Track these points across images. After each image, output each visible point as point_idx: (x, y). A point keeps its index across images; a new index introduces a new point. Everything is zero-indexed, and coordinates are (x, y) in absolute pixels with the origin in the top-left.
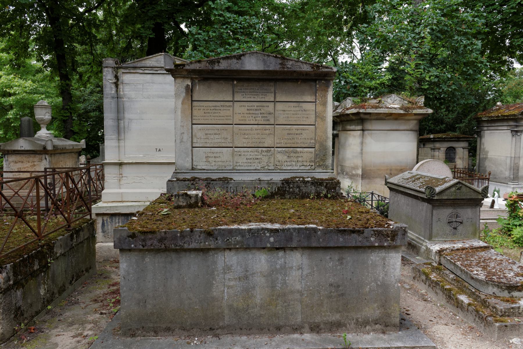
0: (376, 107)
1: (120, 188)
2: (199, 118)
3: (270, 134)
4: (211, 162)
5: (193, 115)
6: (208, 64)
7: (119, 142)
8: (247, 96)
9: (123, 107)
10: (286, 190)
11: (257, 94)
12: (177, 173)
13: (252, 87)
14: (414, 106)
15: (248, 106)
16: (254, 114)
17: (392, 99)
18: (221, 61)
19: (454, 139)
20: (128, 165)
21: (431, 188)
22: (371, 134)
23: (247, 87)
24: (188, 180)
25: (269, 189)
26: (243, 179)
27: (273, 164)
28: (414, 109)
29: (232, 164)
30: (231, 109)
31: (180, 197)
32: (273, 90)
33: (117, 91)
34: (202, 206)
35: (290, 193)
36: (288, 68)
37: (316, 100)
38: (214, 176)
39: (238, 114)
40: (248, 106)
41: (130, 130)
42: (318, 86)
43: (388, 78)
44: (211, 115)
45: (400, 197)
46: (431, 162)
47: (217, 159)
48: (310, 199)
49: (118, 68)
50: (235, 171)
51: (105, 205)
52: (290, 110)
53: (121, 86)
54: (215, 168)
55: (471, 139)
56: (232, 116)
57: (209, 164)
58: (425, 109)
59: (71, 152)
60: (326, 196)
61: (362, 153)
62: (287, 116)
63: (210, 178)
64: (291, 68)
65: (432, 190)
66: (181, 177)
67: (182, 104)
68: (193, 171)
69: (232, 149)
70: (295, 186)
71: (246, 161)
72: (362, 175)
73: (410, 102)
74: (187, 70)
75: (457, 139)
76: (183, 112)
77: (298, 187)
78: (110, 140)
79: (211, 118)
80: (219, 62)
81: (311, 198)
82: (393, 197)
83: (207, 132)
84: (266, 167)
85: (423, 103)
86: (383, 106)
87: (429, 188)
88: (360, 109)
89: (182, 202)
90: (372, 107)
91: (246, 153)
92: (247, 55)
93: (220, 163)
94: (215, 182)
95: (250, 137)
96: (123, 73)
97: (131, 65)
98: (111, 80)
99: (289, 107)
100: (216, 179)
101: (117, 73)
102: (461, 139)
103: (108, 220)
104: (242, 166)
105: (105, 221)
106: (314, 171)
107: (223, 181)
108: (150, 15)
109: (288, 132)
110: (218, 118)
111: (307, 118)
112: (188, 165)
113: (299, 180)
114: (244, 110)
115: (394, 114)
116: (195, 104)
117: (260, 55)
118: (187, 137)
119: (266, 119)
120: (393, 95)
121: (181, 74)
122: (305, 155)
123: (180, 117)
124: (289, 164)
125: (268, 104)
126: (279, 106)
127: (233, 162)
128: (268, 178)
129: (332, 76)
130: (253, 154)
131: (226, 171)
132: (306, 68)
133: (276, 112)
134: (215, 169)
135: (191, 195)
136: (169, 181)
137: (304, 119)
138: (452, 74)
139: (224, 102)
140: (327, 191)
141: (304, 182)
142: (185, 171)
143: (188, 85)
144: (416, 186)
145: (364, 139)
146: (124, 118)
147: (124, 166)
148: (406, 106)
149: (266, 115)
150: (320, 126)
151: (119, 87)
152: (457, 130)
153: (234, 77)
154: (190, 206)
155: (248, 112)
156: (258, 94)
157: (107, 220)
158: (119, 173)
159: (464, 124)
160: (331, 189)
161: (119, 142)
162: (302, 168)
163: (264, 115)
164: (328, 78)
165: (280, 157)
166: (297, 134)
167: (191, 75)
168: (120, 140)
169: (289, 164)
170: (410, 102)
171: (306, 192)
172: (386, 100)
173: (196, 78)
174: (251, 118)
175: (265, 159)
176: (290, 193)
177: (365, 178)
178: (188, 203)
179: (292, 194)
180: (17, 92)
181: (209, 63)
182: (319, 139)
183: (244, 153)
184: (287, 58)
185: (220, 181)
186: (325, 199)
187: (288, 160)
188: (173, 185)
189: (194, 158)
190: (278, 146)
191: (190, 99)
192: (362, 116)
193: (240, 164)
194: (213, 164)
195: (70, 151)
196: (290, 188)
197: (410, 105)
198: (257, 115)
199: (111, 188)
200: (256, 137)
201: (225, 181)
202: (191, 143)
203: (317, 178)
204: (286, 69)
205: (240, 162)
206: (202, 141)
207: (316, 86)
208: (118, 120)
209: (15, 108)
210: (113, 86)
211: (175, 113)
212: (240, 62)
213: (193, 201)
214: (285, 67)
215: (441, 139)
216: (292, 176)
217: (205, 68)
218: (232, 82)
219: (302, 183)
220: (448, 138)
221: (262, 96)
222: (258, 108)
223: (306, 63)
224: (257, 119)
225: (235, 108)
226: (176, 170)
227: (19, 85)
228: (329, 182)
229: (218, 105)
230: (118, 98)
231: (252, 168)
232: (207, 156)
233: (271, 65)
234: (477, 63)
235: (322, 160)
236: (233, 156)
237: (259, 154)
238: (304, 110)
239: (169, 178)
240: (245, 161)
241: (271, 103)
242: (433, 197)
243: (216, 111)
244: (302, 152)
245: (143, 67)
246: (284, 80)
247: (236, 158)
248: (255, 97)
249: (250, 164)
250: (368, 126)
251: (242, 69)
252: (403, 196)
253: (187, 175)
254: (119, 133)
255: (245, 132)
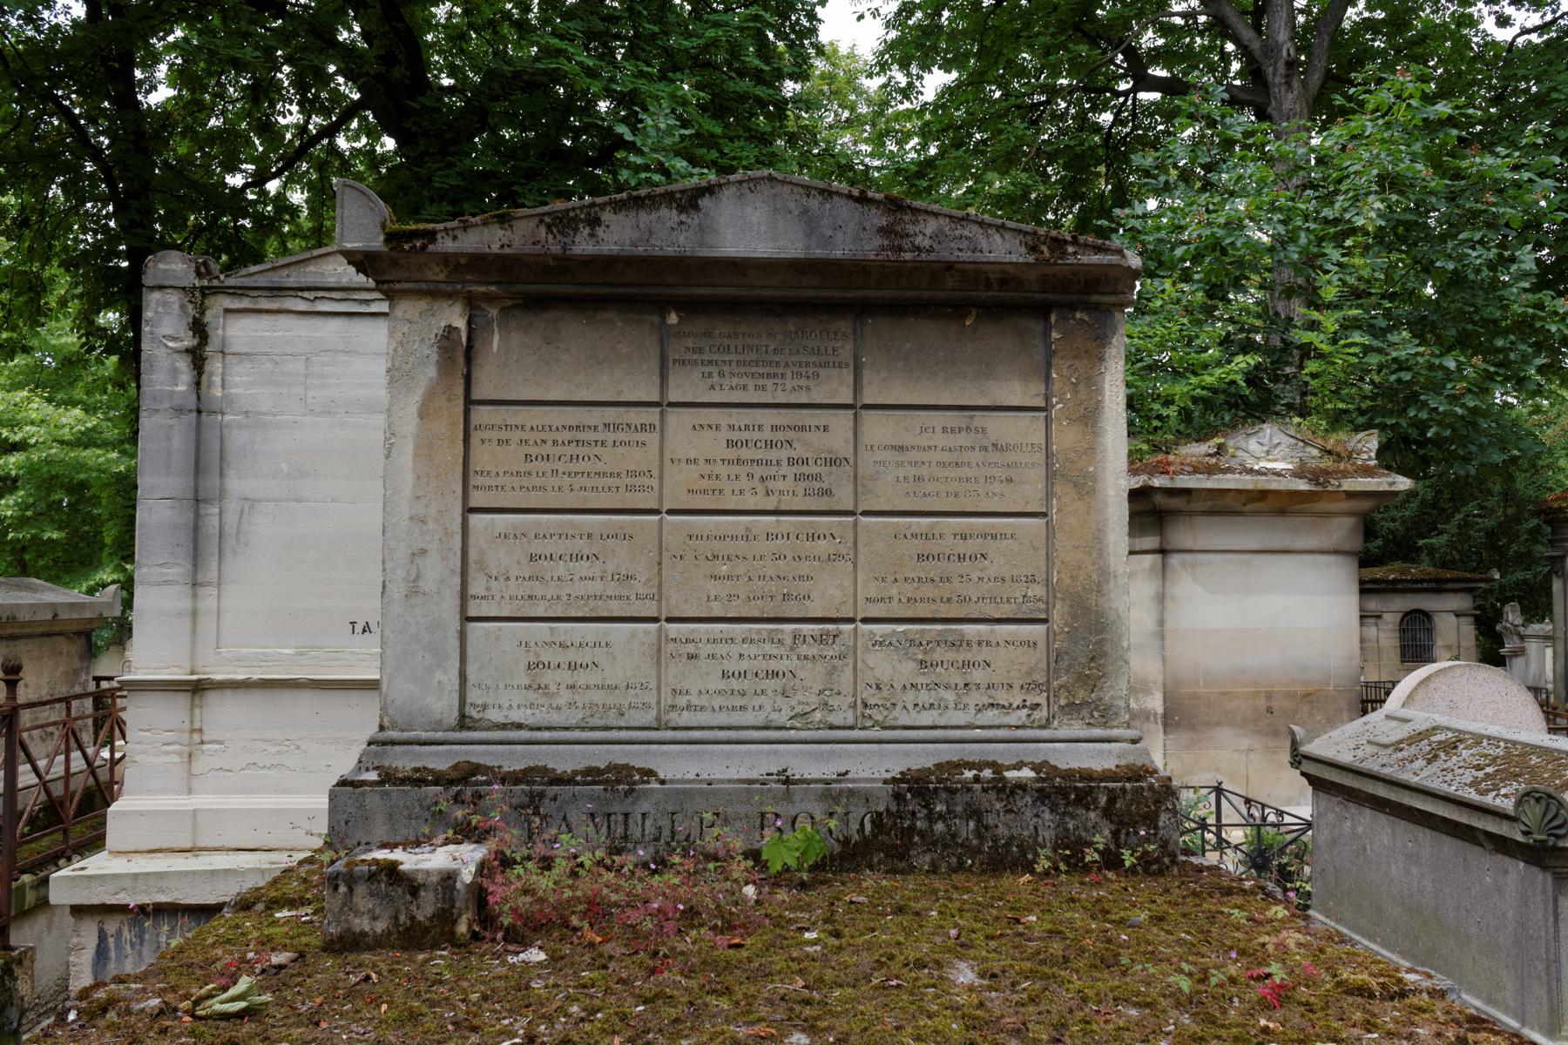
0: (1210, 471)
1: (190, 791)
2: (501, 481)
3: (834, 557)
4: (553, 688)
5: (472, 468)
6: (543, 230)
7: (195, 596)
8: (726, 382)
9: (222, 451)
10: (912, 828)
11: (771, 370)
12: (384, 743)
13: (750, 342)
14: (1342, 466)
15: (732, 427)
16: (758, 462)
17: (1265, 441)
18: (607, 216)
19: (1425, 585)
20: (229, 693)
21: (1550, 796)
22: (1194, 565)
23: (726, 342)
24: (439, 779)
25: (833, 824)
26: (704, 776)
27: (850, 700)
28: (1345, 474)
29: (653, 701)
30: (653, 439)
31: (361, 889)
32: (846, 352)
33: (198, 384)
34: (475, 937)
35: (934, 843)
36: (918, 249)
37: (1047, 399)
38: (565, 761)
39: (683, 465)
40: (732, 427)
41: (246, 545)
42: (1055, 335)
43: (1243, 365)
44: (561, 467)
45: (1367, 822)
46: (1458, 672)
47: (582, 677)
48: (1032, 872)
49: (205, 292)
50: (669, 735)
51: (118, 866)
52: (925, 443)
53: (214, 366)
54: (574, 717)
55: (1482, 585)
56: (655, 472)
57: (542, 701)
58: (1384, 475)
59: (49, 635)
60: (1111, 860)
61: (1161, 634)
62: (913, 471)
63: (544, 770)
64: (931, 250)
65: (1553, 809)
66: (403, 762)
67: (422, 415)
68: (465, 735)
69: (653, 626)
70: (959, 809)
71: (721, 685)
72: (1165, 716)
73: (1329, 453)
74: (446, 259)
75: (1433, 585)
76: (425, 450)
77: (975, 813)
78: (159, 584)
79: (556, 481)
80: (594, 222)
81: (1039, 869)
82: (1331, 817)
83: (537, 547)
84: (818, 715)
85: (1373, 455)
86: (1234, 463)
87: (1538, 800)
88: (1151, 474)
89: (369, 918)
90: (1196, 470)
91: (721, 649)
92: (728, 192)
93: (597, 697)
94: (569, 789)
95: (740, 571)
96: (227, 311)
97: (262, 281)
98: (174, 339)
99: (923, 430)
100: (575, 773)
101: (203, 313)
102: (1449, 586)
103: (126, 934)
104: (702, 708)
105: (111, 940)
106: (1045, 734)
107: (606, 782)
108: (438, 185)
109: (916, 546)
110: (588, 483)
111: (1010, 480)
112: (443, 706)
113: (977, 779)
114: (712, 445)
115: (1275, 492)
116: (481, 415)
117: (787, 189)
118: (439, 572)
119: (816, 485)
120: (1265, 426)
121: (419, 276)
122: (1000, 657)
123: (408, 478)
124: (924, 697)
125: (823, 417)
126: (878, 428)
127: (659, 688)
128: (828, 770)
129: (1120, 288)
130: (753, 650)
131: (624, 735)
132: (1003, 250)
133: (864, 456)
134: (573, 722)
135: (420, 878)
136: (343, 783)
137: (996, 487)
138: (1462, 359)
139: (622, 409)
140: (1115, 834)
141: (1000, 791)
142: (424, 735)
143: (450, 330)
144: (1455, 778)
145: (1168, 585)
146: (222, 494)
147: (212, 697)
148: (1313, 464)
149: (814, 470)
150: (1072, 521)
151: (207, 368)
152: (1424, 556)
153: (669, 291)
154: (412, 937)
155: (732, 454)
156: (780, 370)
157: (119, 933)
158: (187, 726)
159: (1446, 537)
160: (1134, 824)
161: (195, 596)
162: (990, 716)
163: (805, 470)
164: (1104, 299)
165: (884, 666)
166: (961, 558)
167: (463, 282)
168: (201, 585)
169: (924, 697)
170: (1329, 453)
171: (1012, 838)
172: (1242, 444)
173: (490, 299)
174: (745, 483)
175: (813, 676)
176: (934, 843)
177: (1178, 725)
178: (402, 918)
179: (945, 847)
180: (33, 441)
181: (549, 226)
182: (1067, 581)
183: (709, 649)
184: (918, 203)
185: (594, 783)
186: (1110, 875)
187: (921, 680)
188: (362, 806)
189: (471, 670)
190: (875, 611)
191: (460, 391)
192: (1159, 500)
193: (695, 700)
194: (564, 697)
195: (40, 630)
196: (931, 818)
197: (1327, 463)
198: (773, 470)
199: (150, 791)
200: (771, 572)
201: (618, 782)
202: (458, 601)
203: (1062, 766)
204: (908, 256)
205: (694, 691)
206: (513, 588)
207: (1046, 335)
208: (197, 500)
209: (23, 489)
210: (183, 364)
211: (387, 457)
212: (693, 220)
213: (426, 908)
214: (906, 244)
215: (1384, 585)
216: (945, 758)
217: (529, 249)
218: (656, 319)
219: (992, 795)
220: (1406, 581)
221: (796, 383)
222: (780, 436)
223: (1003, 226)
224: (771, 484)
225: (669, 436)
226: (382, 728)
227: (42, 421)
228: (1123, 790)
229: (592, 423)
230: (199, 412)
231: (749, 718)
232: (533, 659)
233: (840, 235)
234: (1542, 319)
235: (1082, 679)
236: (659, 662)
237: (782, 651)
238: (995, 445)
239: (345, 765)
240: (716, 683)
241: (841, 412)
242: (1558, 837)
243: (582, 451)
244: (988, 643)
245: (309, 289)
246: (899, 309)
247: (672, 671)
248: (763, 388)
249: (739, 702)
250: (1181, 535)
251: (705, 253)
252: (1382, 817)
253: (436, 754)
254: (196, 557)
255: (717, 546)
